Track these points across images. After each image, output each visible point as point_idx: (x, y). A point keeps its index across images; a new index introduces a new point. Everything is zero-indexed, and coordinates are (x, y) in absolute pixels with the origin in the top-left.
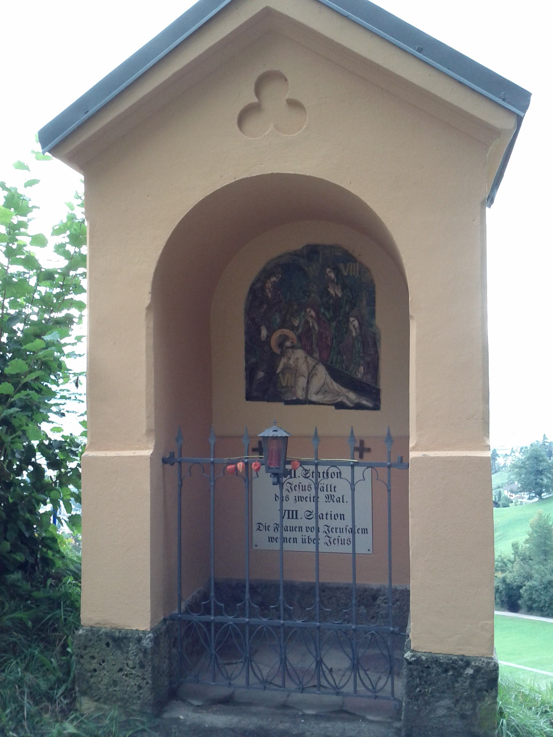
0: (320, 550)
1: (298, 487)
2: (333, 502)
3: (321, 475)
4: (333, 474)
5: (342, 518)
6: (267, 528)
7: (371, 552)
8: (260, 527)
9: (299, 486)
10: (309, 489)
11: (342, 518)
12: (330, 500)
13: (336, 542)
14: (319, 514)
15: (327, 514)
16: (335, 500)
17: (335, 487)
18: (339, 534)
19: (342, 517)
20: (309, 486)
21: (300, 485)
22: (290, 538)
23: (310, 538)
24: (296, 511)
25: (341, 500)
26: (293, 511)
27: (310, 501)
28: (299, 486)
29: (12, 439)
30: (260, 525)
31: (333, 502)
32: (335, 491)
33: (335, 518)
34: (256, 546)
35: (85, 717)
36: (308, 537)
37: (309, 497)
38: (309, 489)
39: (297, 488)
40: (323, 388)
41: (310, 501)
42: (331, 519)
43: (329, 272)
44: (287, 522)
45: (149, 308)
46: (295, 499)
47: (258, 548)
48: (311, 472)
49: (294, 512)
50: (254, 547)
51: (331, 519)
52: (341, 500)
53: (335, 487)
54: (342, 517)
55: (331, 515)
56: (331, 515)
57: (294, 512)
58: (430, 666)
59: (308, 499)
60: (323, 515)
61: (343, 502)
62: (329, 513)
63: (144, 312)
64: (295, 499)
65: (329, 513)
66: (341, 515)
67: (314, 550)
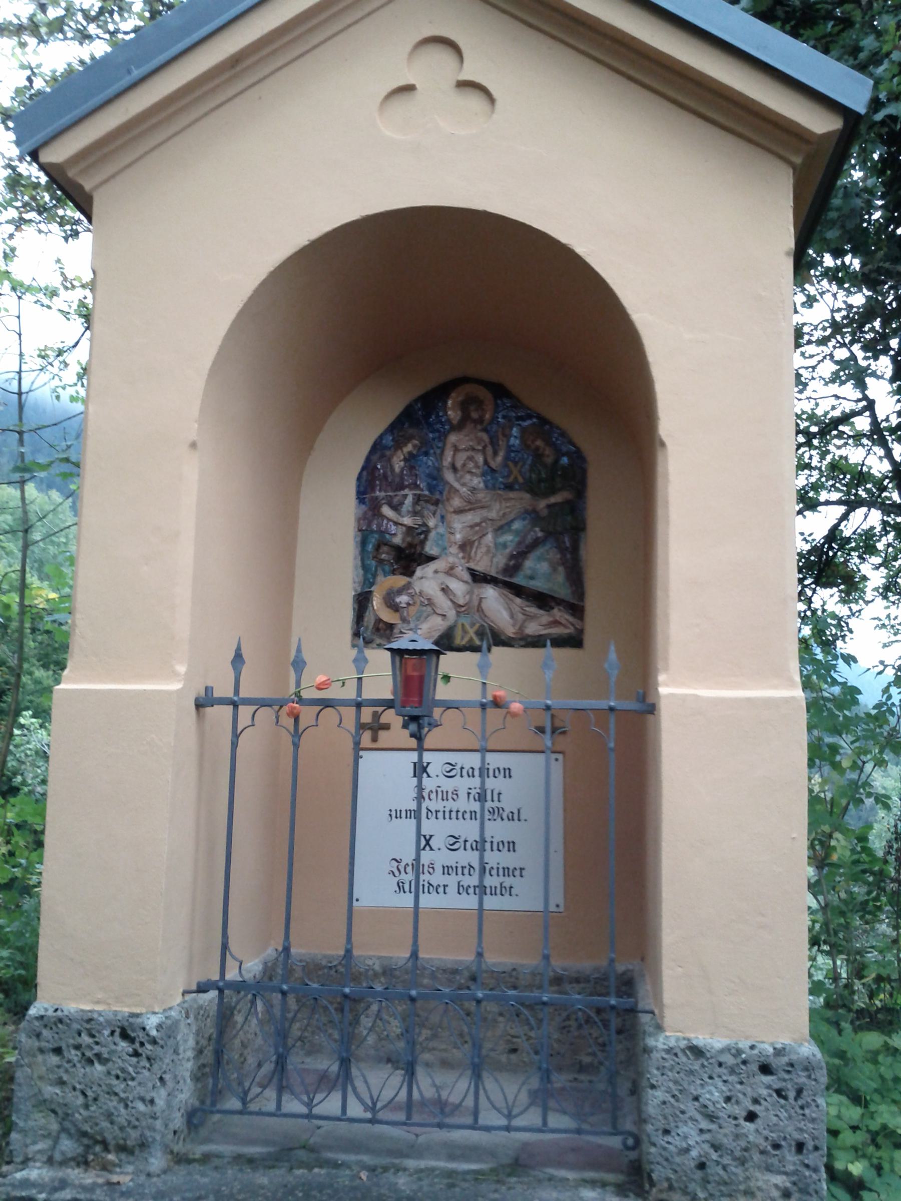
0: (485, 907)
1: (435, 794)
2: (502, 819)
4: (497, 772)
5: (511, 849)
7: (561, 909)
9: (437, 792)
11: (511, 849)
12: (495, 817)
16: (505, 816)
17: (499, 794)
18: (501, 879)
21: (439, 790)
22: (469, 886)
23: (461, 884)
24: (444, 874)
25: (516, 817)
27: (444, 818)
28: (437, 792)
31: (502, 819)
32: (499, 801)
36: (501, 884)
37: (442, 809)
39: (433, 796)
40: (533, 629)
41: (444, 818)
42: (492, 850)
43: (548, 456)
46: (390, 815)
48: (458, 767)
51: (492, 850)
52: (516, 817)
53: (499, 794)
55: (492, 842)
56: (492, 842)
58: (159, 1076)
59: (440, 815)
61: (519, 820)
64: (390, 815)
66: (509, 843)
67: (475, 906)
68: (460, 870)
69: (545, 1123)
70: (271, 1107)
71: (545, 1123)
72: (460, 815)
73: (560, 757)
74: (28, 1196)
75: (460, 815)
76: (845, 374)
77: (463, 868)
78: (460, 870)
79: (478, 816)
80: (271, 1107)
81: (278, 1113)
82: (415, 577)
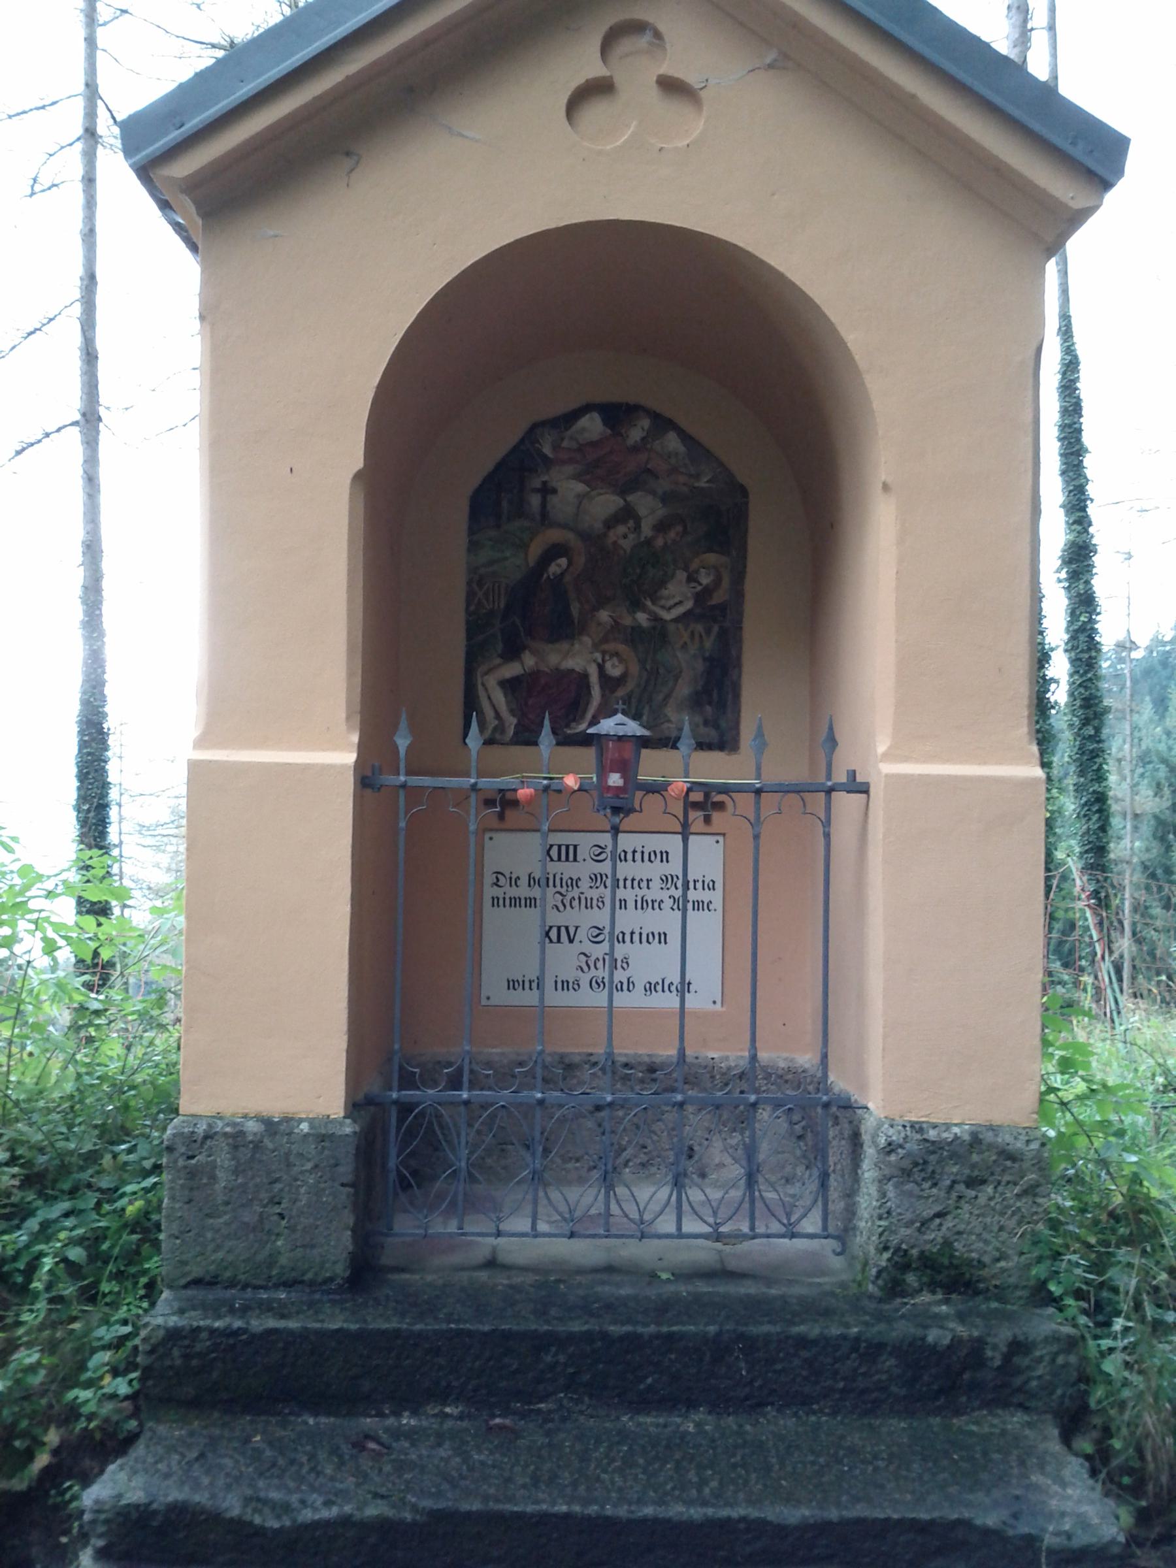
0: (615, 1004)
3: (621, 883)
6: (515, 882)
8: (498, 879)
9: (580, 898)
10: (600, 904)
12: (598, 884)
13: (575, 903)
14: (619, 851)
15: (634, 852)
19: (665, 856)
20: (601, 900)
21: (583, 897)
24: (575, 847)
26: (567, 847)
28: (580, 898)
29: (99, 1221)
30: (500, 876)
32: (648, 888)
33: (648, 941)
34: (491, 839)
35: (54, 1403)
38: (600, 904)
44: (554, 868)
45: (358, 476)
47: (493, 1002)
49: (571, 849)
50: (484, 1002)
54: (665, 856)
55: (641, 934)
56: (641, 934)
57: (571, 849)
60: (624, 934)
62: (639, 849)
63: (349, 481)
65: (637, 931)
68: (527, 985)
69: (679, 1228)
70: (671, 1228)
71: (679, 1228)
72: (636, 883)
73: (721, 839)
74: (941, 1518)
75: (636, 883)
76: (447, 1460)
77: (530, 982)
78: (527, 985)
79: (618, 903)
80: (671, 1228)
81: (680, 1235)
82: (707, 1180)
